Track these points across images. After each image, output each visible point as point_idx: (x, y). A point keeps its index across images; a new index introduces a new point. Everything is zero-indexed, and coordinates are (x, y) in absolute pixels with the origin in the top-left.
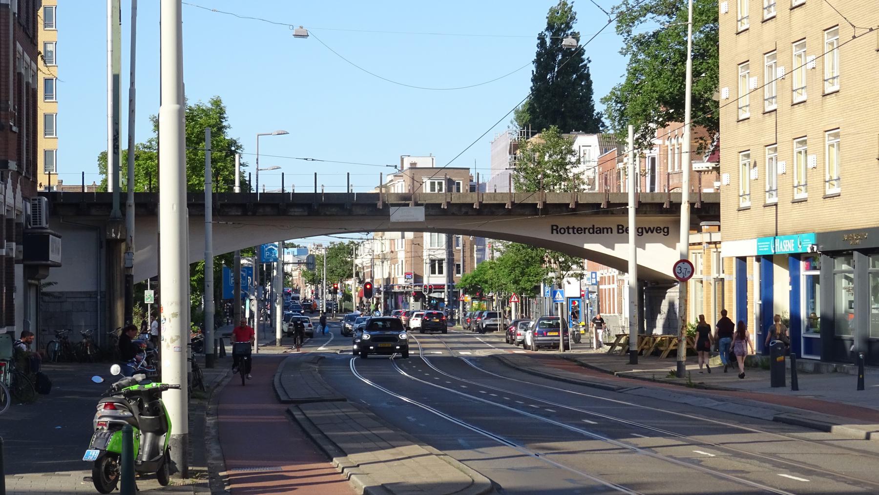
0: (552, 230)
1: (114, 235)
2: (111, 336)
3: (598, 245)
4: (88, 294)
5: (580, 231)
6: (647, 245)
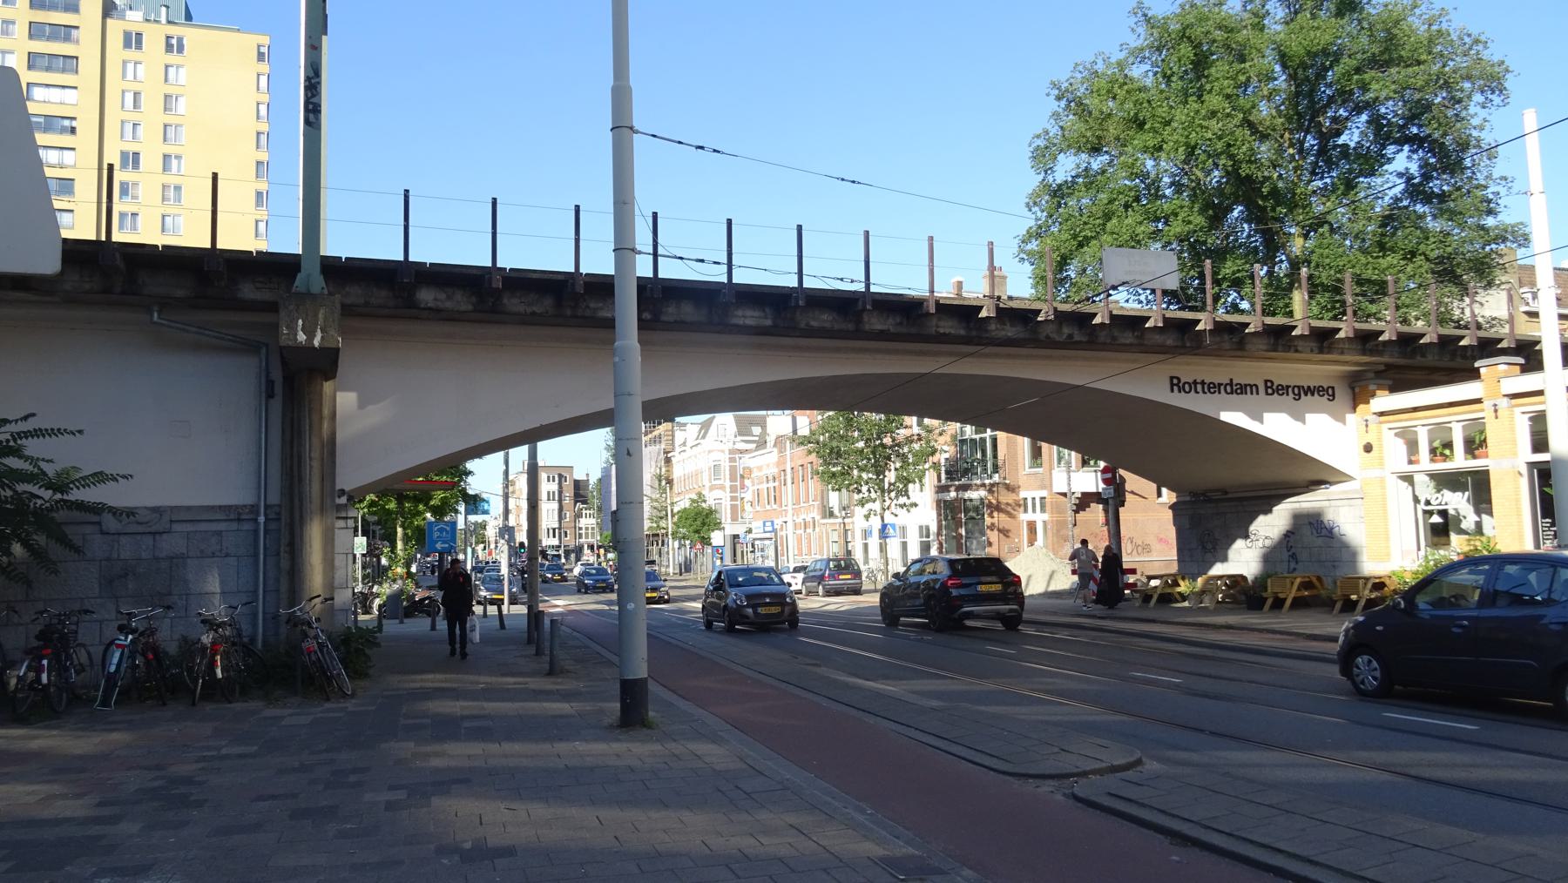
0: (1172, 385)
1: (302, 337)
2: (293, 621)
3: (1240, 414)
4: (234, 514)
5: (1213, 388)
6: (1308, 416)
